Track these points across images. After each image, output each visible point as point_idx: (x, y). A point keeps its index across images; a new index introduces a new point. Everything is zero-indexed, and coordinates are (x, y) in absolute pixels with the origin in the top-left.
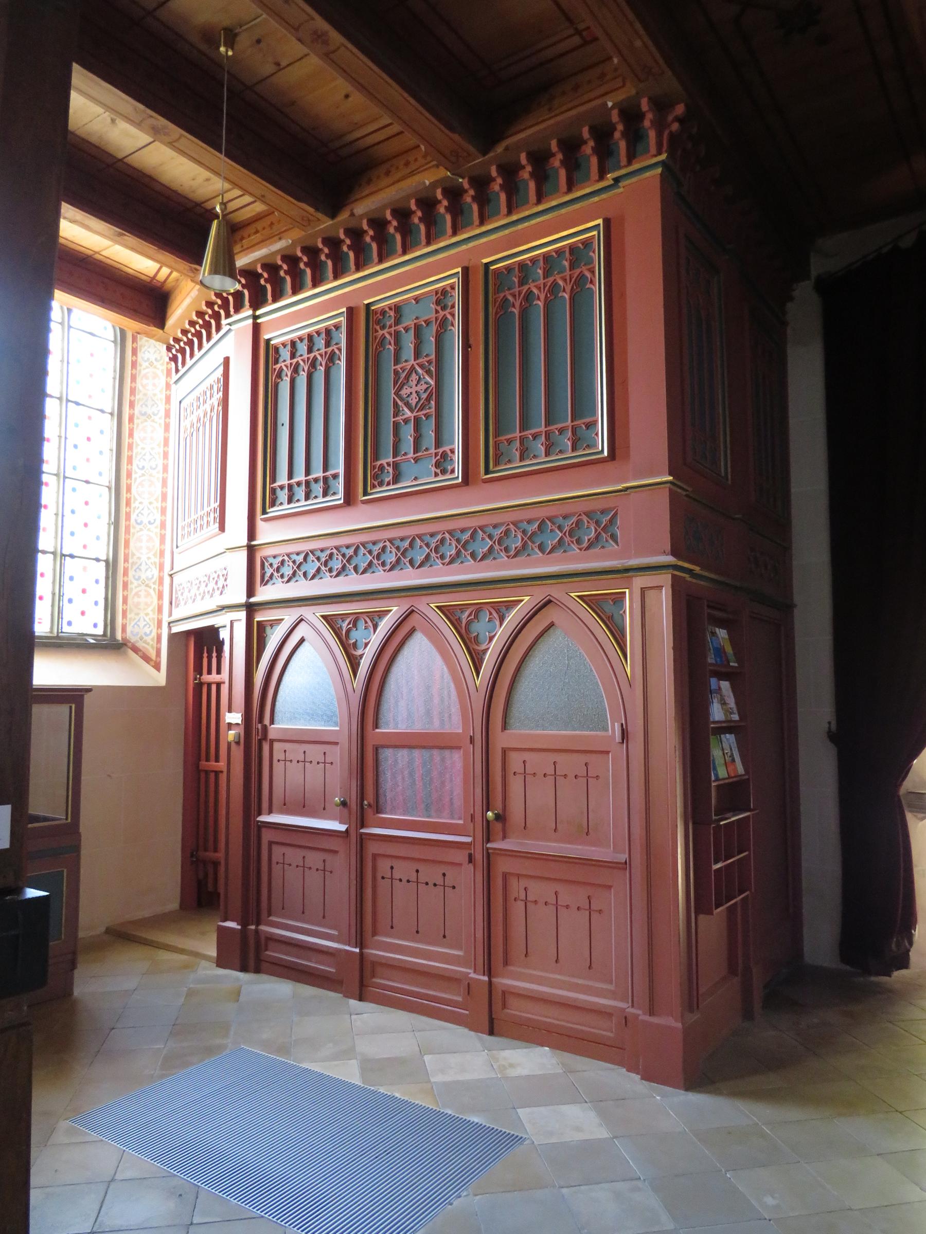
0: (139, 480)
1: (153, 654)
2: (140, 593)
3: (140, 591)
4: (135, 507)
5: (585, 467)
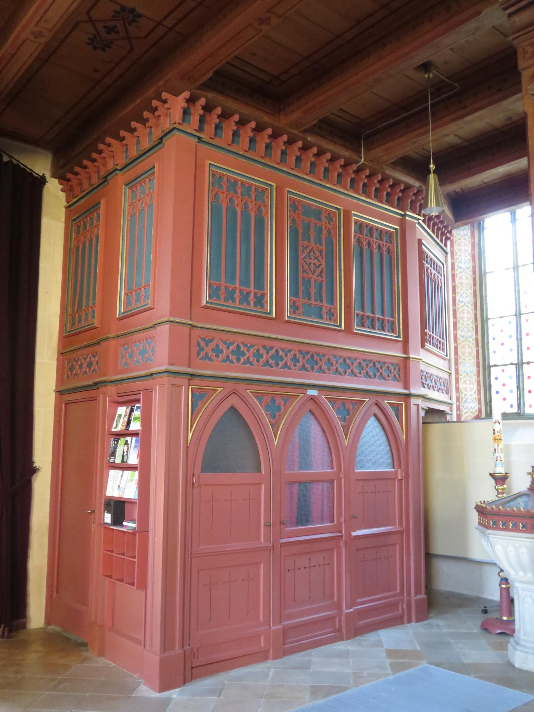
0: (460, 309)
2: (462, 277)
3: (462, 275)
4: (458, 292)
5: (319, 329)
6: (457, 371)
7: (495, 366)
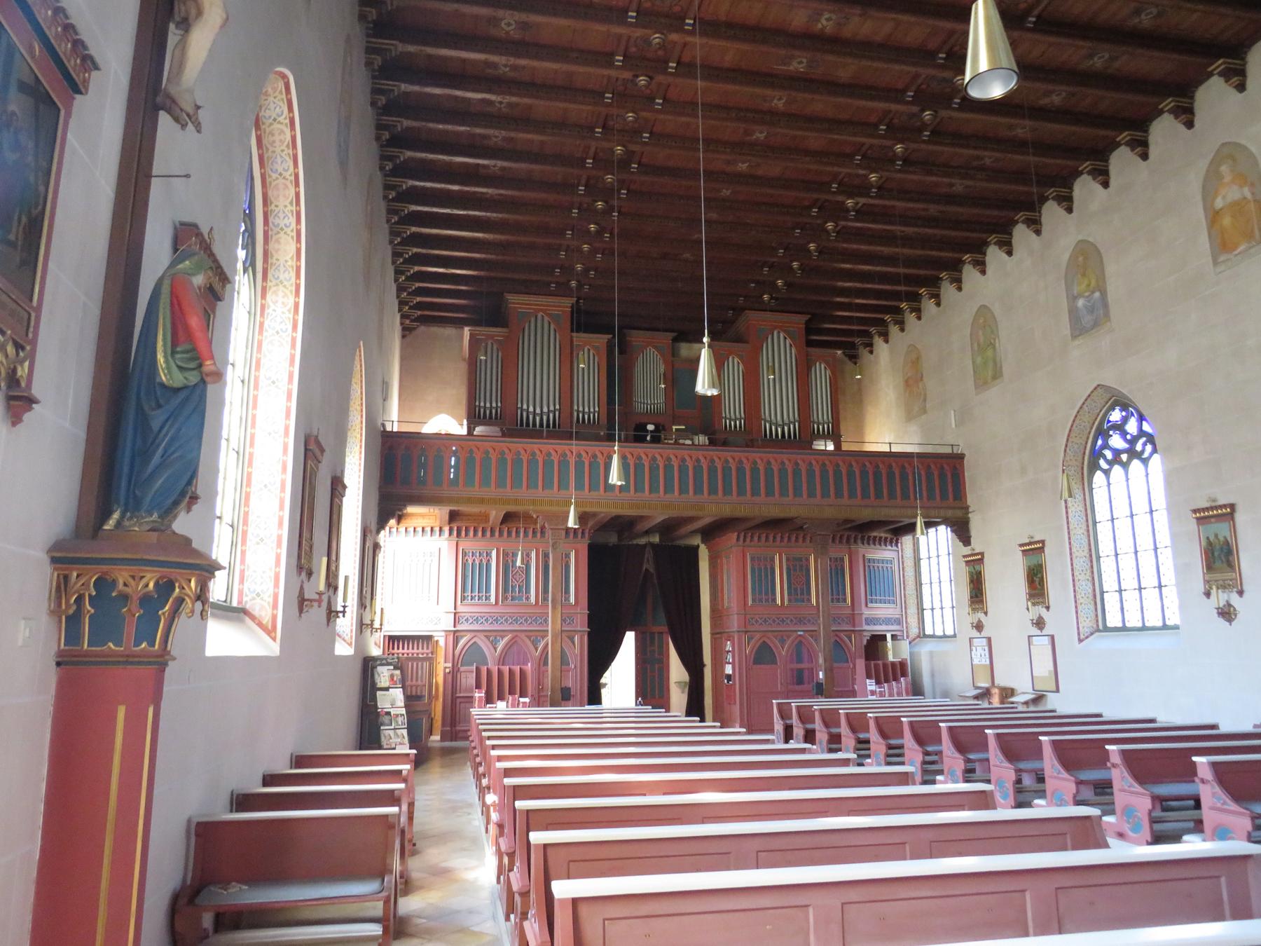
1: (266, 619)
6: (906, 612)
7: (944, 631)
